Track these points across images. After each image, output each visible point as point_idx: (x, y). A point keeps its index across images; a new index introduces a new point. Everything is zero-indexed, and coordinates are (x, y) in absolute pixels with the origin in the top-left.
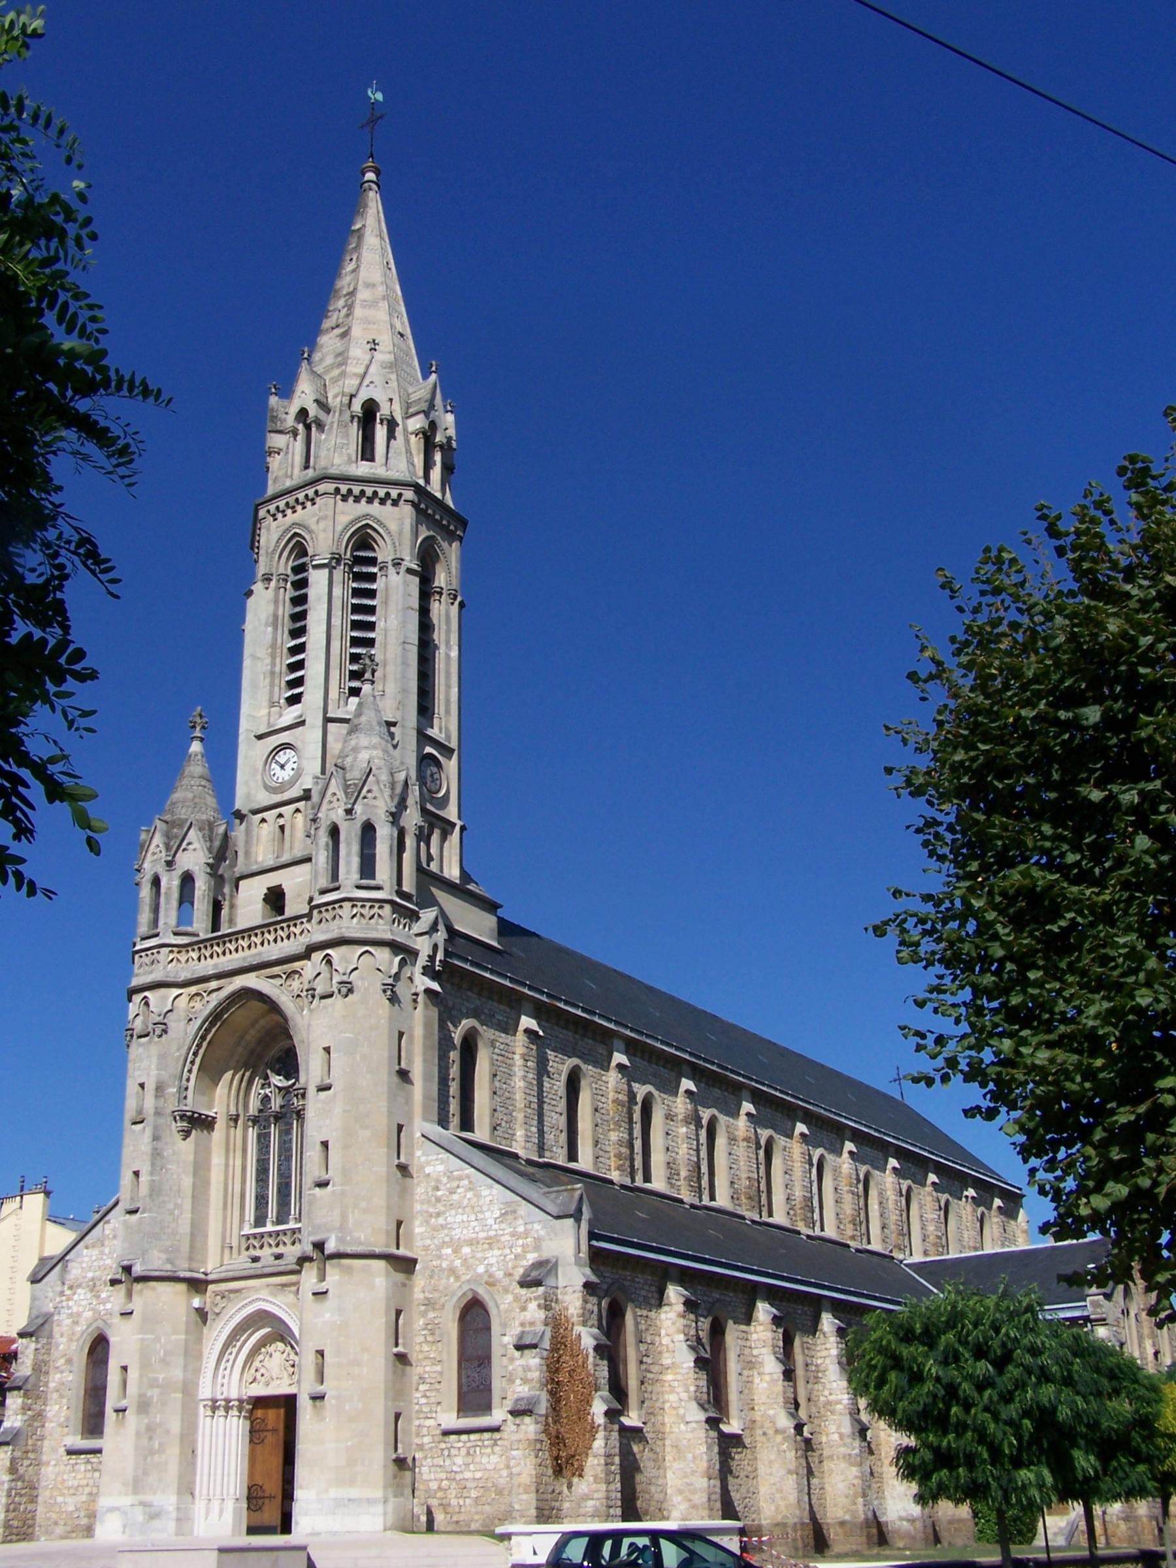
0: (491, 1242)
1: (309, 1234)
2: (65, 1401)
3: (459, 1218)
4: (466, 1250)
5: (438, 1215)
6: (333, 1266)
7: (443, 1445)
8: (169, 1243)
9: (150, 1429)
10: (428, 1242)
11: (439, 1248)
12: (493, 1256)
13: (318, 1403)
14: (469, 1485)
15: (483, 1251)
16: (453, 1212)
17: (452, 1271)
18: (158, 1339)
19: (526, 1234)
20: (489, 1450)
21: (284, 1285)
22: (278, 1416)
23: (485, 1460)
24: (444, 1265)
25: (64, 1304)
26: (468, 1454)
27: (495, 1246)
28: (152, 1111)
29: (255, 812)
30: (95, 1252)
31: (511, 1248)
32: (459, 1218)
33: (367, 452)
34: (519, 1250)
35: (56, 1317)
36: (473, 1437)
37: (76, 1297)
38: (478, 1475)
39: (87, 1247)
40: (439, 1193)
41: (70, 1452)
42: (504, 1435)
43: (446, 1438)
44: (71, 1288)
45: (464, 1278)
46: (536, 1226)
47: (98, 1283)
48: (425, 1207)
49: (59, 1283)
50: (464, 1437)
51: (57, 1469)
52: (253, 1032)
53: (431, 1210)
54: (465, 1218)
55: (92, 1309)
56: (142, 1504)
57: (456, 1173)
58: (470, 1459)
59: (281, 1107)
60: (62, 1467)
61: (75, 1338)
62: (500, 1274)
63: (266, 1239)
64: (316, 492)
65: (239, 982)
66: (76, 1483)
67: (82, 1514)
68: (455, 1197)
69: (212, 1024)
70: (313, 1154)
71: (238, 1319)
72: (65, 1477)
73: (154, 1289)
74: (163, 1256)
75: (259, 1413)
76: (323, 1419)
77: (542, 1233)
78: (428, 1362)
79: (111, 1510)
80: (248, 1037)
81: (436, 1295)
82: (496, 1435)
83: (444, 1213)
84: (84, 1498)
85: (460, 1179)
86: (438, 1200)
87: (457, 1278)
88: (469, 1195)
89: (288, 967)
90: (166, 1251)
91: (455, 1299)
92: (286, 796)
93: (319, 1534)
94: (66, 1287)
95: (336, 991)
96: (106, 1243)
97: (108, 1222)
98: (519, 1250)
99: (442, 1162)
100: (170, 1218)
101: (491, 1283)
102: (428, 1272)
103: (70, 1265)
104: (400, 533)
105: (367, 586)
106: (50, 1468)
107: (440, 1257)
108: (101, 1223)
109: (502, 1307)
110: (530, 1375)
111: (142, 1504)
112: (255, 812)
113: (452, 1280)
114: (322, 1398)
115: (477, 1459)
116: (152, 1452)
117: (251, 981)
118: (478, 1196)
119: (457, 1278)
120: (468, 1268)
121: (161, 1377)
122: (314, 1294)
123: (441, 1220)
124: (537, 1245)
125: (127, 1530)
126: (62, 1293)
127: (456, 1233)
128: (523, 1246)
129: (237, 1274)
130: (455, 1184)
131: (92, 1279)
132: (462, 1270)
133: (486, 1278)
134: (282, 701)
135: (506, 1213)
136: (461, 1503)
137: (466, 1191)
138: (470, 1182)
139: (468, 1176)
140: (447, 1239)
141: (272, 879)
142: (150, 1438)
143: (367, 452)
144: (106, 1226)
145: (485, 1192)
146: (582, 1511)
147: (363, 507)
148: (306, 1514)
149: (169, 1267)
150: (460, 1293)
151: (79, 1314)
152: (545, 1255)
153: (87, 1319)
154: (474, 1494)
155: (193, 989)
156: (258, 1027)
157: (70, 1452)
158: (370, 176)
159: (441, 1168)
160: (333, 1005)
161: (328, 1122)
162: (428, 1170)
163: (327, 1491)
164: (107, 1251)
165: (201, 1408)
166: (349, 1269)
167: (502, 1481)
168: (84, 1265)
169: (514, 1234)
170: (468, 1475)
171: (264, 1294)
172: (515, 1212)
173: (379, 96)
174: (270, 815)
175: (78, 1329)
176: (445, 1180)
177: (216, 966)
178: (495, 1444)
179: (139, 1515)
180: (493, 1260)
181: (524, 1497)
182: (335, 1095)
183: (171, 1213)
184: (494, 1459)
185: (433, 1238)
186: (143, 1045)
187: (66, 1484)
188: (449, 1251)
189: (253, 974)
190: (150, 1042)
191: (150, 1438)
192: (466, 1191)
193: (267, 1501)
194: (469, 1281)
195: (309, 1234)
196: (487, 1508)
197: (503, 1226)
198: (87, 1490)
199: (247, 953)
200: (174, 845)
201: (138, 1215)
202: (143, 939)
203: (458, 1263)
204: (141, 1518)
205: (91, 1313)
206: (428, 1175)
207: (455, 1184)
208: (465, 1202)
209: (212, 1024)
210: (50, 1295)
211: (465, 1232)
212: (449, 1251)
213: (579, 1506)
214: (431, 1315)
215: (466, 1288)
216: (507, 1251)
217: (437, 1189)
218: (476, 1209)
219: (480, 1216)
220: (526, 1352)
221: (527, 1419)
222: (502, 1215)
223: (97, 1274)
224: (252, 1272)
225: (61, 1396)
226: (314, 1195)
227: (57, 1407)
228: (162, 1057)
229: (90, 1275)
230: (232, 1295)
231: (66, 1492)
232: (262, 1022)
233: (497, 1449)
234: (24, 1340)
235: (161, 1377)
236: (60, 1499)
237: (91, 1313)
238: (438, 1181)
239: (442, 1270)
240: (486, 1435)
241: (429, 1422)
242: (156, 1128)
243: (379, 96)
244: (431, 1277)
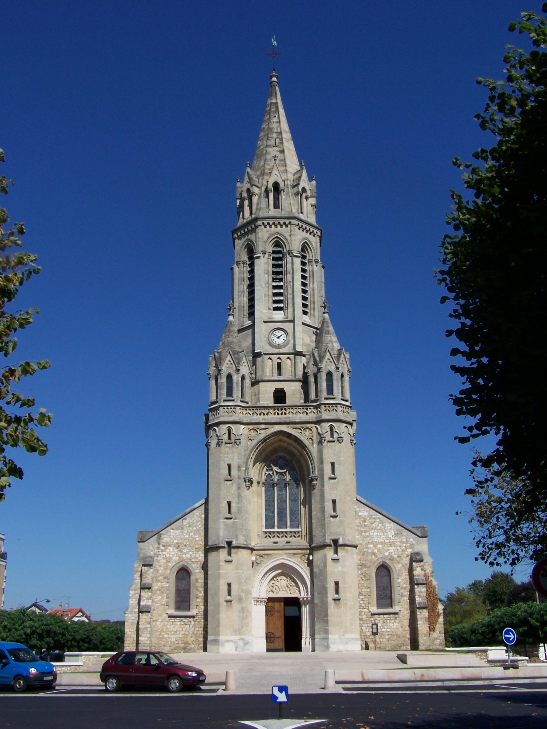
0: (391, 544)
1: (328, 536)
2: (165, 595)
3: (376, 534)
4: (380, 546)
5: (366, 532)
6: (341, 549)
7: (372, 619)
8: (244, 533)
9: (243, 609)
10: (362, 542)
11: (367, 544)
12: (392, 549)
13: (337, 602)
14: (384, 634)
15: (387, 547)
16: (373, 531)
17: (373, 554)
18: (243, 573)
19: (407, 542)
20: (393, 621)
21: (294, 554)
22: (280, 606)
23: (391, 625)
24: (370, 551)
25: (160, 553)
26: (384, 622)
27: (393, 545)
28: (236, 477)
29: (265, 354)
30: (178, 532)
31: (400, 547)
32: (376, 534)
33: (277, 206)
34: (404, 548)
35: (156, 558)
36: (385, 616)
37: (168, 550)
38: (389, 630)
39: (173, 529)
40: (366, 523)
41: (170, 617)
42: (400, 616)
43: (373, 616)
44: (164, 546)
45: (379, 557)
46: (411, 540)
47: (181, 545)
48: (359, 528)
49: (157, 543)
50: (381, 616)
51: (163, 623)
52: (270, 448)
53: (362, 529)
54: (379, 534)
55: (178, 556)
56: (242, 639)
57: (373, 516)
58: (385, 624)
59: (278, 480)
60: (166, 623)
61: (169, 568)
62: (396, 556)
63: (276, 534)
64: (290, 223)
65: (277, 428)
66: (175, 630)
67: (180, 642)
68: (374, 525)
69: (262, 443)
70: (329, 506)
71: (271, 566)
72: (168, 627)
73: (241, 552)
74: (243, 538)
75: (270, 604)
76: (340, 608)
77: (414, 542)
78: (364, 587)
79: (228, 641)
80: (268, 450)
81: (367, 562)
82: (397, 616)
83: (368, 531)
84: (181, 636)
85: (375, 519)
86: (365, 526)
87: (376, 556)
88: (380, 525)
89: (305, 426)
90: (244, 536)
91: (390, 564)
92: (282, 351)
93: (341, 651)
94: (161, 546)
95: (336, 440)
96: (185, 528)
97: (185, 519)
98: (404, 548)
99: (367, 511)
100: (245, 523)
101: (392, 559)
102: (361, 553)
103: (163, 536)
104: (316, 249)
105: (276, 263)
106: (159, 623)
107: (367, 548)
108: (181, 520)
109: (397, 568)
110: (422, 594)
111: (242, 639)
112: (265, 354)
113: (373, 557)
114: (339, 600)
115: (388, 624)
116: (243, 619)
117: (284, 428)
118: (385, 526)
119: (376, 556)
120: (381, 553)
121: (245, 588)
122: (332, 559)
123: (367, 534)
124: (412, 546)
125: (238, 649)
126: (158, 548)
127: (375, 539)
128: (405, 546)
129: (267, 548)
130: (373, 520)
131: (177, 543)
132: (378, 554)
133: (389, 557)
134: (272, 308)
135: (397, 534)
136: (381, 640)
137: (379, 523)
138: (380, 520)
139: (379, 518)
140: (370, 541)
141: (280, 385)
142: (243, 613)
143: (277, 206)
144: (184, 521)
145: (387, 525)
146: (435, 643)
147: (308, 235)
148: (334, 644)
149: (245, 543)
150: (378, 562)
151: (170, 558)
152: (416, 550)
153: (175, 561)
154: (387, 637)
155: (251, 427)
156: (273, 446)
157: (170, 617)
158: (275, 79)
159: (366, 514)
160: (335, 445)
161: (335, 492)
162: (360, 514)
163: (344, 635)
164: (185, 532)
165: (253, 602)
166: (347, 551)
167: (399, 633)
168: (172, 537)
169: (401, 542)
170: (383, 630)
171: (285, 557)
172: (401, 533)
173: (275, 43)
174: (274, 357)
175: (171, 565)
176: (368, 519)
177: (264, 419)
178: (396, 619)
179: (241, 644)
180: (391, 551)
181: (425, 638)
182: (338, 482)
183: (245, 521)
184: (395, 624)
185: (363, 540)
186: (229, 447)
187: (169, 630)
188: (372, 546)
189: (285, 426)
190: (233, 446)
191: (243, 613)
192: (379, 523)
193: (276, 639)
194: (382, 558)
195: (328, 536)
196: (393, 642)
197: (396, 538)
198: (182, 632)
199: (266, 416)
200: (237, 363)
201: (232, 520)
202: (224, 401)
203: (376, 551)
204: (242, 645)
205: (177, 558)
206: (360, 516)
207: (373, 520)
208: (378, 528)
209: (262, 443)
210: (151, 548)
211: (379, 539)
212: (372, 546)
213: (434, 641)
214: (364, 570)
215: (381, 560)
216: (399, 548)
217: (365, 521)
218: (384, 531)
219: (385, 534)
220: (420, 586)
221: (425, 610)
222: (395, 534)
223: (180, 541)
224: (286, 547)
225: (162, 593)
226: (330, 520)
227: (160, 597)
228: (239, 454)
229: (176, 541)
230: (266, 556)
231: (170, 633)
232: (276, 445)
233: (397, 621)
234: (146, 568)
235: (245, 588)
236: (166, 636)
237: (177, 558)
238: (365, 518)
239: (368, 553)
240: (392, 616)
241: (366, 610)
242: (239, 484)
243: (275, 43)
244: (363, 555)
